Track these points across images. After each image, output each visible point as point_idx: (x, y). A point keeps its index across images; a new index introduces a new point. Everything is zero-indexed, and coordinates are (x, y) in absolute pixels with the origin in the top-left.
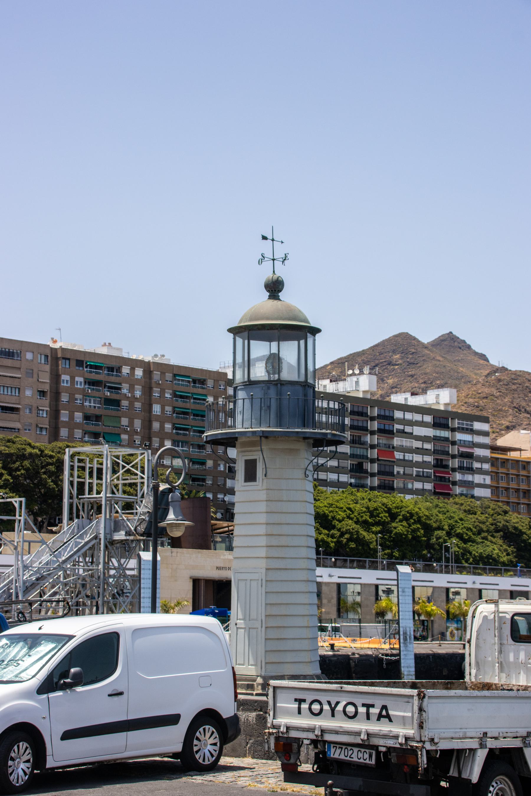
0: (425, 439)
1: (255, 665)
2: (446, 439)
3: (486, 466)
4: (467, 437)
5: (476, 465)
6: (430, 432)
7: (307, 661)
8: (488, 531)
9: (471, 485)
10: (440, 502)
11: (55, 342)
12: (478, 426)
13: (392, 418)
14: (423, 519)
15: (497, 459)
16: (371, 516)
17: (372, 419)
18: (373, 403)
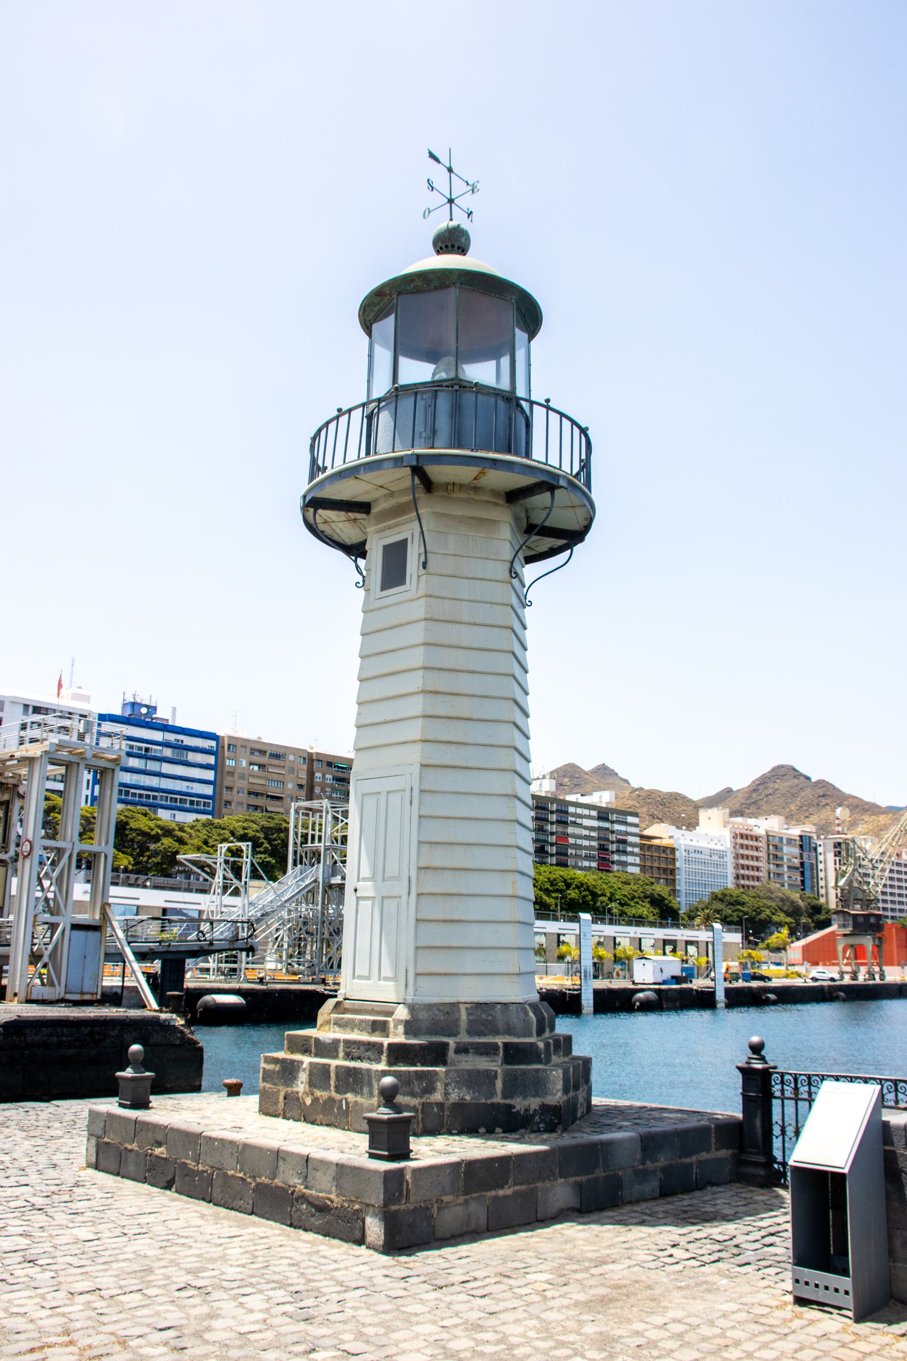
0: (591, 829)
1: (395, 979)
2: (607, 829)
3: (637, 850)
4: (622, 828)
5: (629, 849)
6: (595, 823)
7: (511, 971)
8: (639, 898)
9: (624, 864)
10: (603, 875)
11: (312, 748)
12: (630, 819)
13: (567, 812)
14: (591, 888)
15: (644, 844)
16: (552, 885)
17: (552, 812)
18: (554, 800)
